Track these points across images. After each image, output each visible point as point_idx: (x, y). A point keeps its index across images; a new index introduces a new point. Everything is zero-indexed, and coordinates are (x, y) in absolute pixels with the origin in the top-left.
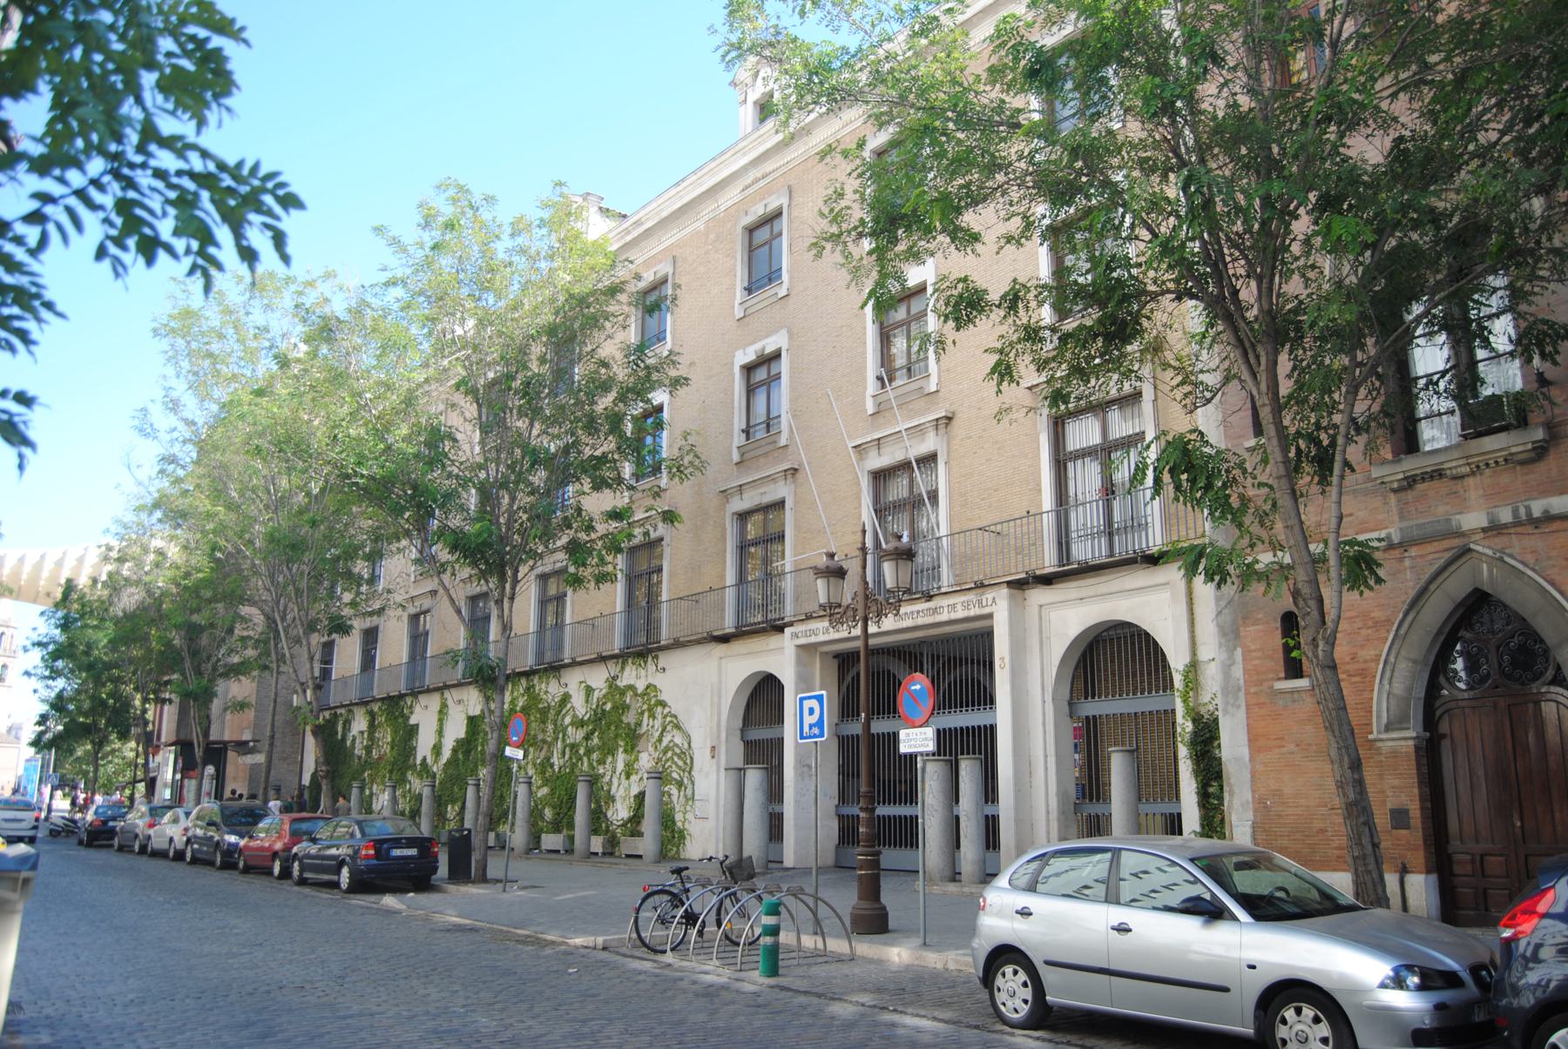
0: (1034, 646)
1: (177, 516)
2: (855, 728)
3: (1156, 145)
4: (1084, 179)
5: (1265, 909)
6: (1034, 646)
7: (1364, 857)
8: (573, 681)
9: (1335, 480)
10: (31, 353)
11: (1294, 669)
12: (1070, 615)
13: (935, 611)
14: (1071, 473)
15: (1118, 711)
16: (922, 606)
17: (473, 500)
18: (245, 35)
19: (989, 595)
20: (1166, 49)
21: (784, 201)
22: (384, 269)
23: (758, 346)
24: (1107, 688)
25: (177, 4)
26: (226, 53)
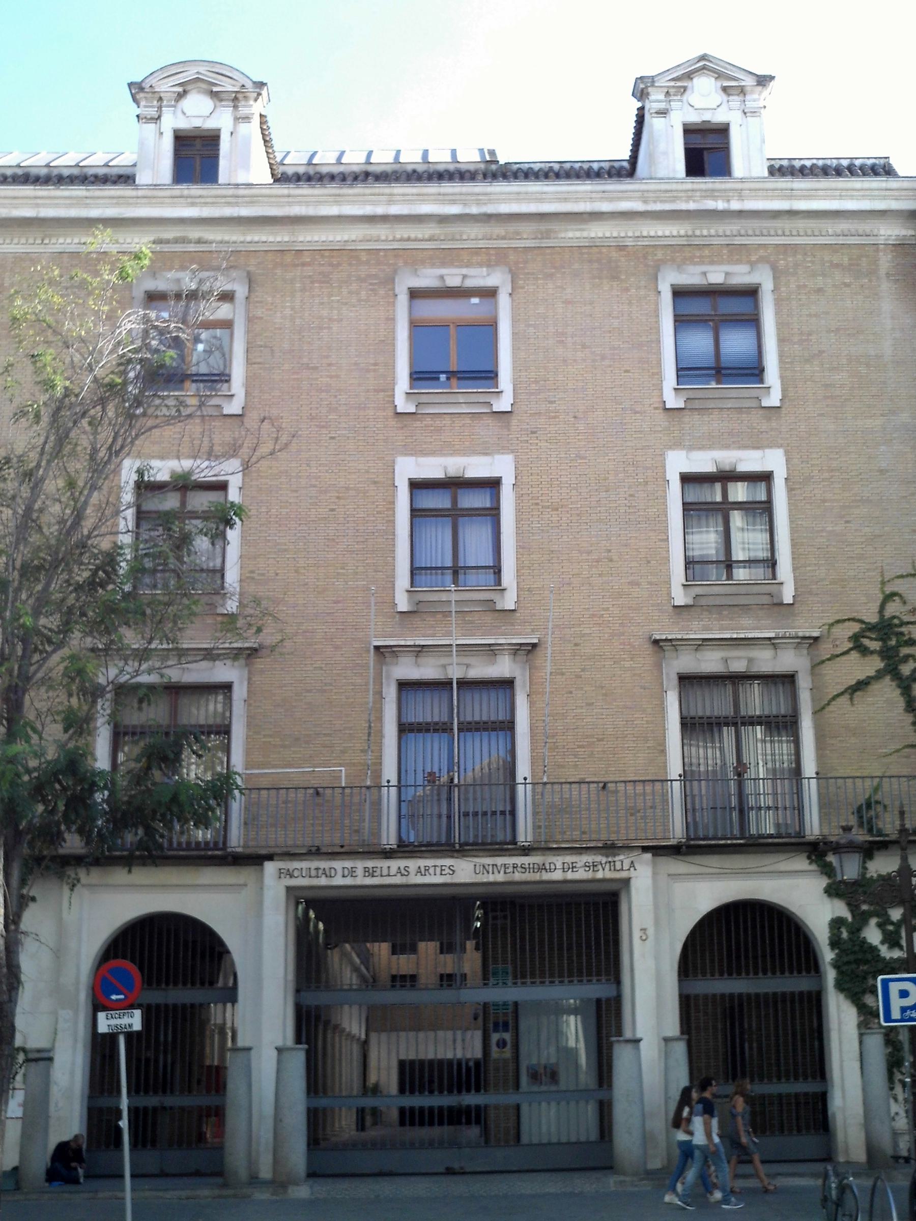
0: (663, 909)
1: (665, 153)
2: (104, 1024)
3: (342, 985)
4: (39, 268)
5: (661, 201)
6: (663, 909)
7: (840, 196)
8: (55, 672)
9: (501, 763)
10: (104, 724)
11: (824, 1207)
12: (707, 890)
13: (542, 868)
14: (732, 710)
15: (770, 990)
16: (181, 245)
17: (458, 937)
18: (847, 696)
19: (623, 859)
20: (380, 787)
21: (563, 1086)
22: (476, 1019)
23: (187, 464)
24: (747, 966)
25: (911, 642)
26: (827, 942)
